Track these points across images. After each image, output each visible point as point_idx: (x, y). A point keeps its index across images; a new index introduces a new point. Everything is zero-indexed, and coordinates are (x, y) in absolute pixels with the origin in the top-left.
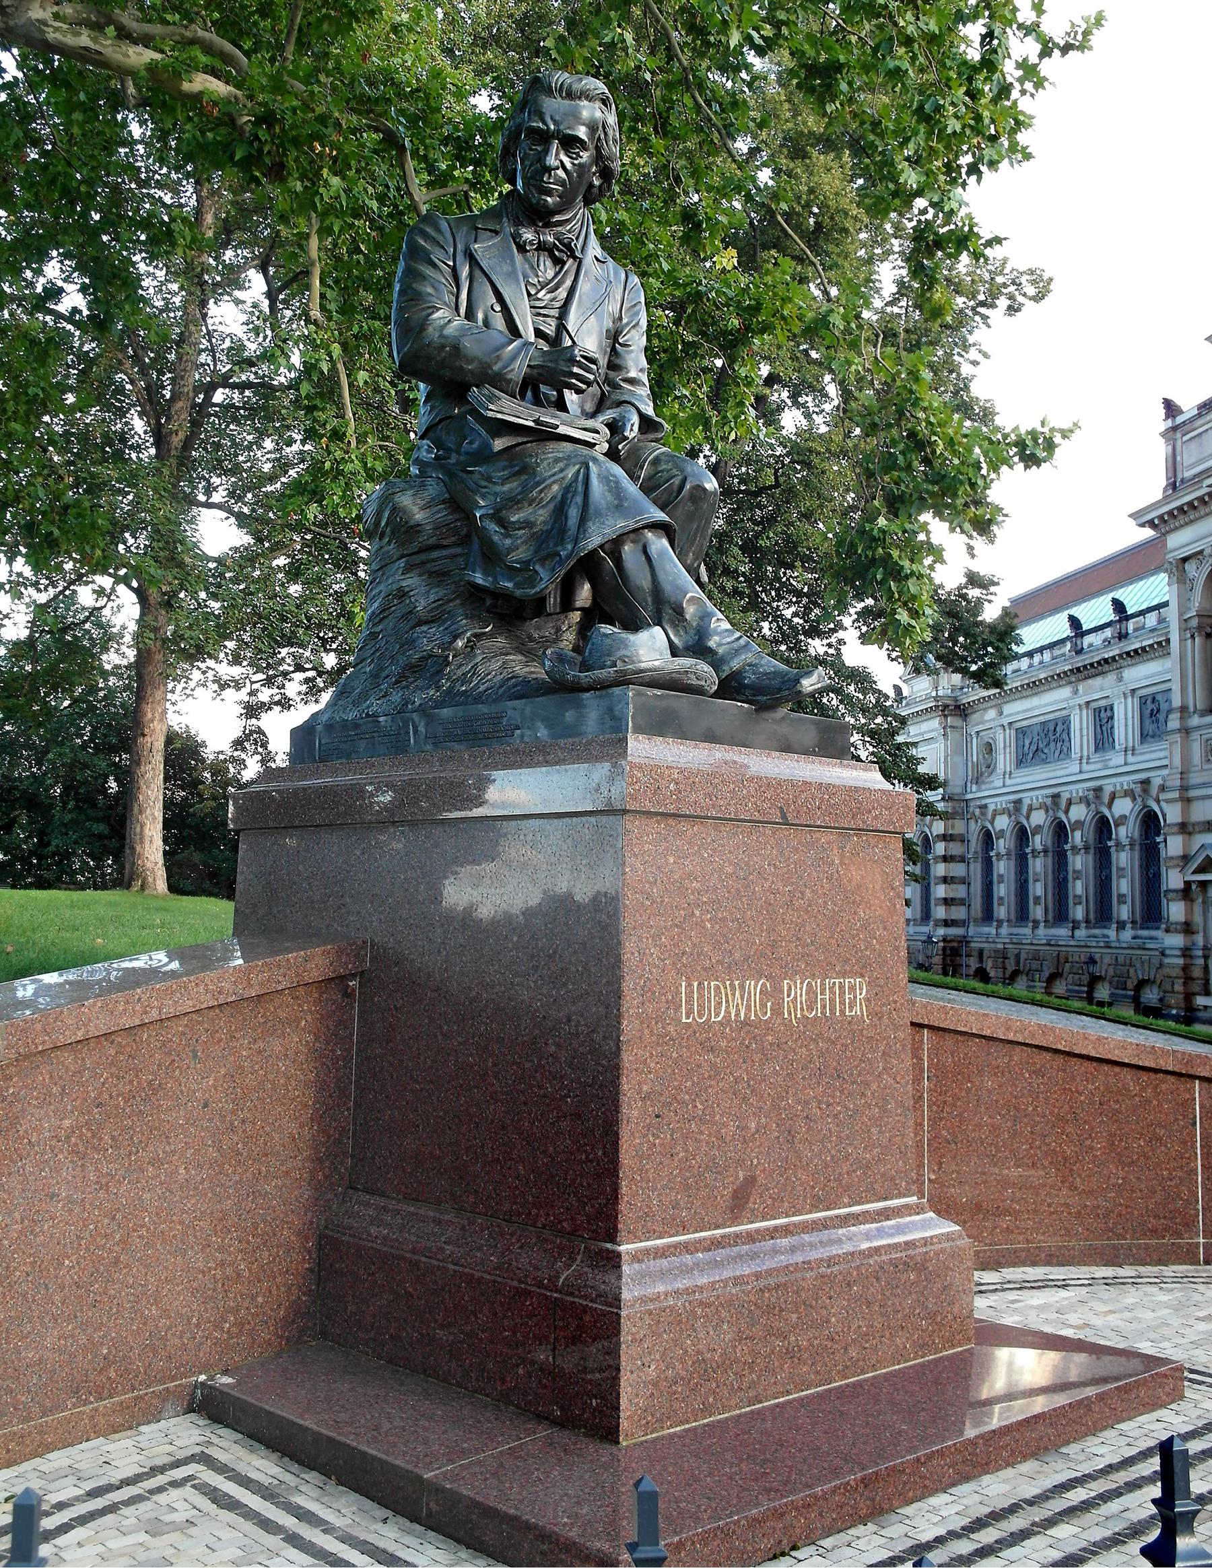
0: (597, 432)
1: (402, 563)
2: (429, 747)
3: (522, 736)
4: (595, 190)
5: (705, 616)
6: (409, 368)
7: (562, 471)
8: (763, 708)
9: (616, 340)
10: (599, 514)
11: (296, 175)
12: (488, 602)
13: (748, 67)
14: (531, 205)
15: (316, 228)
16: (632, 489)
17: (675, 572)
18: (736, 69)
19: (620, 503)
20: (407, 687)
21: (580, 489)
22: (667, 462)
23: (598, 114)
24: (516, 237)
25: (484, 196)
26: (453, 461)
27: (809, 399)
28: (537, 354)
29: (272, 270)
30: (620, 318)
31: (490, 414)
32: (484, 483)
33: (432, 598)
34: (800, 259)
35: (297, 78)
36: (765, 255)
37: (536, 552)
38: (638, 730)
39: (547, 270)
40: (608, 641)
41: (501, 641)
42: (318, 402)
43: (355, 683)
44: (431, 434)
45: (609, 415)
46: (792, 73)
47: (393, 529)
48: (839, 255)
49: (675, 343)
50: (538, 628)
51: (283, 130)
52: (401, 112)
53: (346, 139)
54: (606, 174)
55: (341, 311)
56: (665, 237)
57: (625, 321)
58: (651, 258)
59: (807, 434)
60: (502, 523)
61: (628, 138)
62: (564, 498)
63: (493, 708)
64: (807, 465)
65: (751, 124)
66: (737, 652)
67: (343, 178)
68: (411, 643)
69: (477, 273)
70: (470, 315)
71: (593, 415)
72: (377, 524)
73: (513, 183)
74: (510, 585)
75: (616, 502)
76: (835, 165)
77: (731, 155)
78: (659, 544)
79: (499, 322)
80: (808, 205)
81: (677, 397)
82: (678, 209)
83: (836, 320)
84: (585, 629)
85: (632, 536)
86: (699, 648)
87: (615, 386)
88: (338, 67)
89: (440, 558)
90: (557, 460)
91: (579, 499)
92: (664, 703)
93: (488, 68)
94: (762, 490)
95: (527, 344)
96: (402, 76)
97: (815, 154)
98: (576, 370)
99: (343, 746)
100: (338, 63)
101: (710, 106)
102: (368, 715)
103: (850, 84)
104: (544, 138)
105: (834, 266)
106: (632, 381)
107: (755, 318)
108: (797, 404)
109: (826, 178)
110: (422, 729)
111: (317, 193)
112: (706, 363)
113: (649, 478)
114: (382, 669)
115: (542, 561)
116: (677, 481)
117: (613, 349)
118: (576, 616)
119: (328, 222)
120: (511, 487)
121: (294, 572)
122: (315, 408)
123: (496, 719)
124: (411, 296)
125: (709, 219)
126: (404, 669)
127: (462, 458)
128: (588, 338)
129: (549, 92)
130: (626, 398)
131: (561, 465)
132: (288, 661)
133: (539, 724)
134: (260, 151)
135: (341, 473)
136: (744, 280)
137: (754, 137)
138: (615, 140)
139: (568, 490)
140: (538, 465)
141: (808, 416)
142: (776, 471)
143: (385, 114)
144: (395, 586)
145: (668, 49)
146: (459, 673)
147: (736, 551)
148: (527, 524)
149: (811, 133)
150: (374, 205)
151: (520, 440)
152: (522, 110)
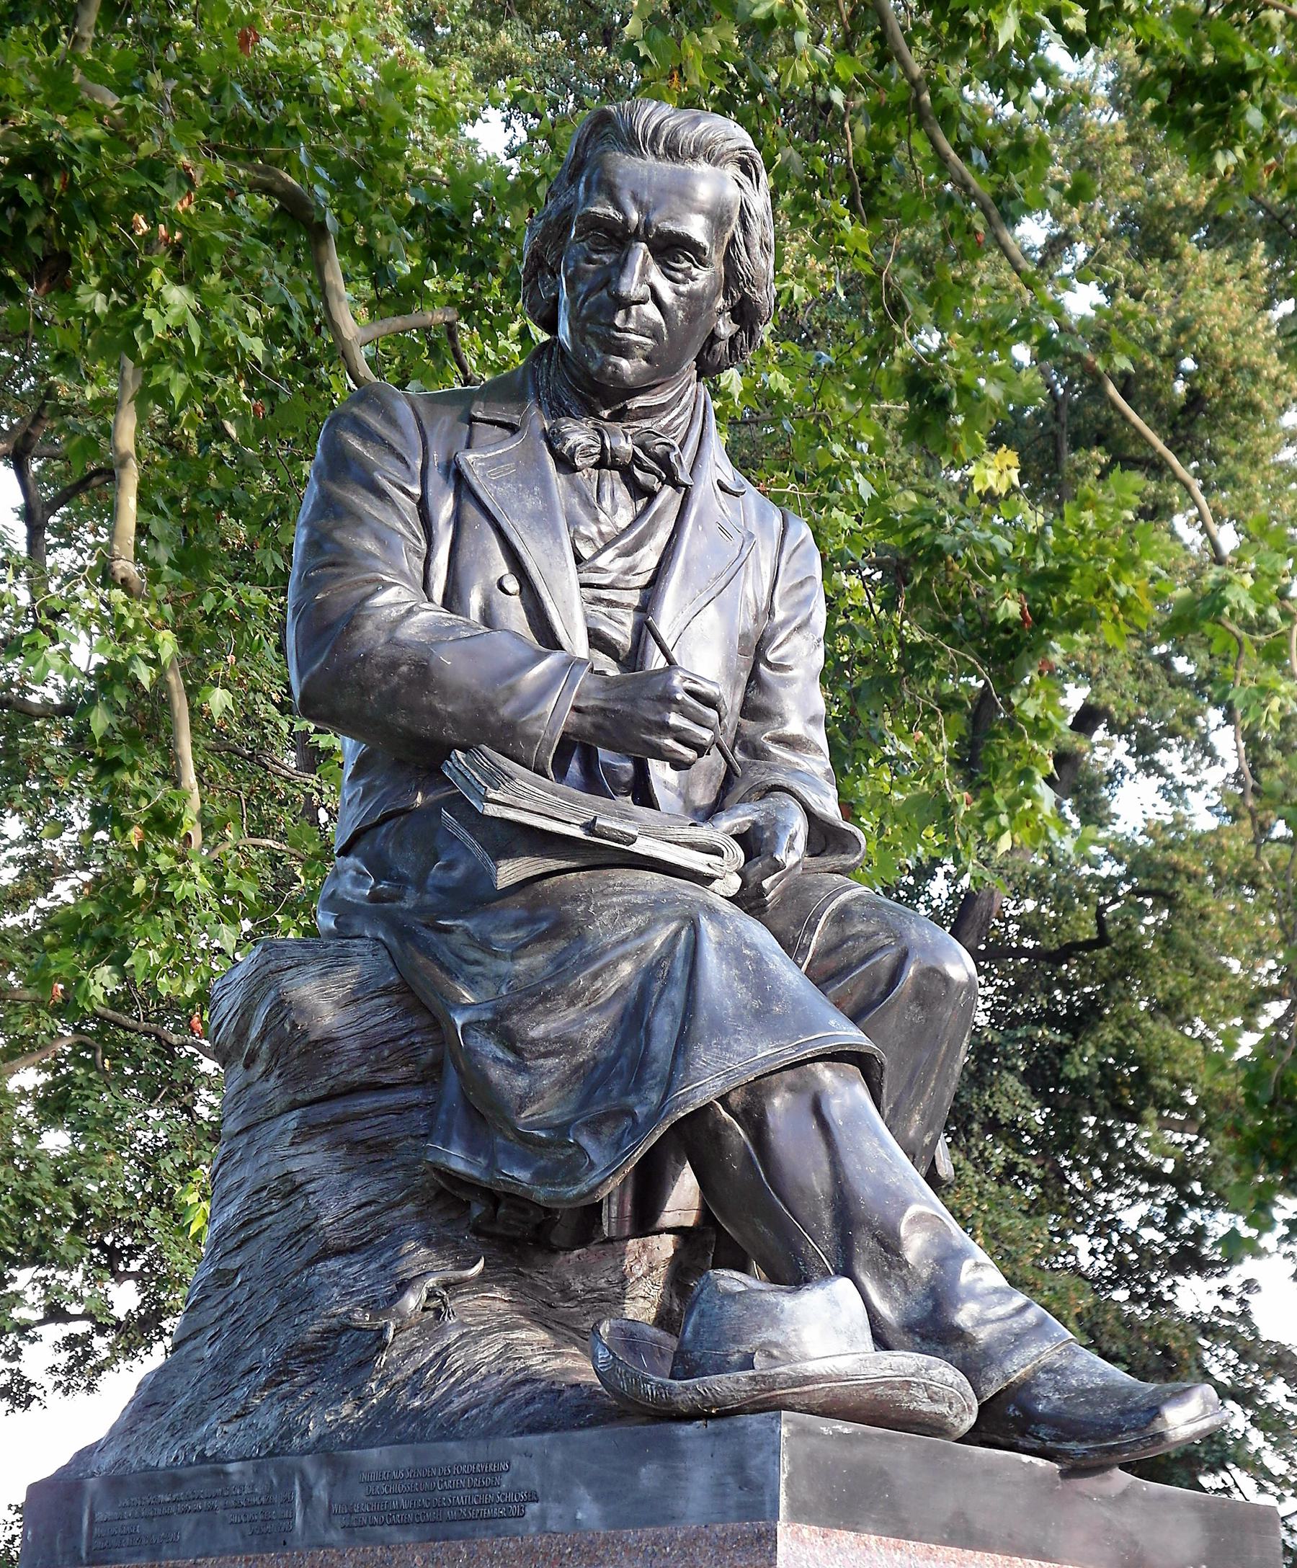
0: (718, 852)
1: (292, 1121)
2: (334, 1536)
3: (543, 1517)
4: (722, 347)
5: (948, 1258)
6: (319, 704)
7: (640, 932)
8: (1076, 1470)
9: (759, 654)
10: (718, 1027)
11: (94, 281)
12: (477, 1211)
13: (1049, 75)
14: (588, 375)
15: (132, 388)
16: (789, 974)
17: (881, 1156)
18: (1025, 81)
19: (764, 1006)
20: (292, 1396)
21: (680, 972)
22: (867, 918)
23: (732, 192)
24: (552, 439)
25: (489, 334)
26: (408, 904)
27: (1177, 755)
28: (592, 684)
29: (35, 466)
30: (770, 611)
31: (491, 810)
32: (474, 955)
33: (355, 1198)
34: (1156, 467)
35: (100, 77)
36: (1077, 458)
37: (584, 1103)
38: (800, 1513)
39: (619, 509)
40: (734, 1309)
41: (498, 1299)
42: (122, 753)
43: (179, 1384)
44: (363, 845)
45: (740, 817)
46: (1142, 88)
47: (279, 1050)
48: (1238, 458)
49: (884, 644)
50: (583, 1270)
51: (70, 186)
52: (319, 156)
53: (203, 208)
54: (745, 314)
55: (179, 563)
56: (867, 432)
57: (780, 616)
58: (833, 474)
59: (1170, 835)
60: (510, 1041)
61: (794, 220)
62: (644, 990)
63: (482, 1451)
64: (1166, 898)
65: (1053, 196)
66: (1018, 1339)
67: (196, 288)
68: (303, 1298)
69: (471, 512)
70: (453, 599)
71: (710, 813)
72: (241, 1034)
73: (550, 325)
74: (523, 1175)
75: (757, 1014)
76: (1233, 272)
77: (1005, 251)
78: (846, 1094)
79: (514, 614)
80: (1173, 356)
81: (886, 758)
82: (897, 367)
83: (1240, 595)
84: (682, 1275)
85: (789, 1076)
86: (933, 1329)
87: (756, 751)
88: (188, 61)
89: (377, 1112)
90: (631, 910)
91: (676, 995)
92: (859, 1452)
93: (502, 67)
94: (1068, 951)
95: (572, 663)
96: (323, 80)
97: (1190, 248)
98: (674, 719)
99: (144, 1528)
100: (190, 49)
101: (965, 154)
102: (202, 1457)
103: (1268, 110)
104: (617, 238)
105: (1230, 480)
106: (792, 743)
107: (1056, 597)
108: (1151, 768)
109: (1214, 299)
110: (321, 1492)
111: (139, 318)
112: (949, 686)
113: (828, 951)
114: (237, 1354)
115: (594, 1127)
116: (886, 959)
117: (754, 676)
118: (665, 1246)
119: (157, 380)
120: (535, 961)
121: (54, 1106)
122: (117, 764)
123: (487, 1475)
124: (329, 556)
125: (964, 390)
126: (287, 1354)
127: (428, 899)
128: (700, 652)
129: (631, 143)
130: (781, 779)
131: (639, 920)
132: (31, 1297)
133: (581, 1492)
134: (19, 227)
135: (165, 900)
136: (1033, 518)
137: (1057, 217)
138: (765, 246)
139: (649, 974)
140: (590, 918)
141: (1174, 793)
142: (1102, 909)
143: (286, 159)
144: (275, 1171)
145: (881, 38)
146: (409, 1368)
147: (1011, 1082)
148: (565, 1044)
149: (1181, 208)
150: (257, 347)
151: (553, 864)
152: (573, 179)
